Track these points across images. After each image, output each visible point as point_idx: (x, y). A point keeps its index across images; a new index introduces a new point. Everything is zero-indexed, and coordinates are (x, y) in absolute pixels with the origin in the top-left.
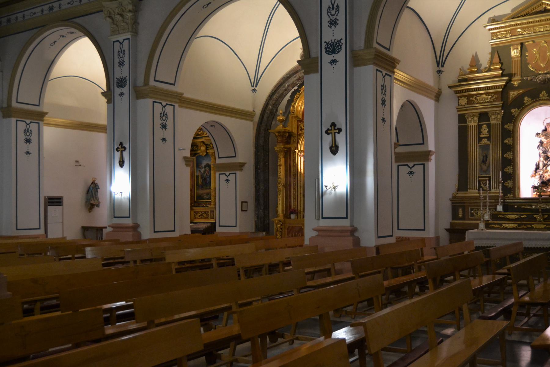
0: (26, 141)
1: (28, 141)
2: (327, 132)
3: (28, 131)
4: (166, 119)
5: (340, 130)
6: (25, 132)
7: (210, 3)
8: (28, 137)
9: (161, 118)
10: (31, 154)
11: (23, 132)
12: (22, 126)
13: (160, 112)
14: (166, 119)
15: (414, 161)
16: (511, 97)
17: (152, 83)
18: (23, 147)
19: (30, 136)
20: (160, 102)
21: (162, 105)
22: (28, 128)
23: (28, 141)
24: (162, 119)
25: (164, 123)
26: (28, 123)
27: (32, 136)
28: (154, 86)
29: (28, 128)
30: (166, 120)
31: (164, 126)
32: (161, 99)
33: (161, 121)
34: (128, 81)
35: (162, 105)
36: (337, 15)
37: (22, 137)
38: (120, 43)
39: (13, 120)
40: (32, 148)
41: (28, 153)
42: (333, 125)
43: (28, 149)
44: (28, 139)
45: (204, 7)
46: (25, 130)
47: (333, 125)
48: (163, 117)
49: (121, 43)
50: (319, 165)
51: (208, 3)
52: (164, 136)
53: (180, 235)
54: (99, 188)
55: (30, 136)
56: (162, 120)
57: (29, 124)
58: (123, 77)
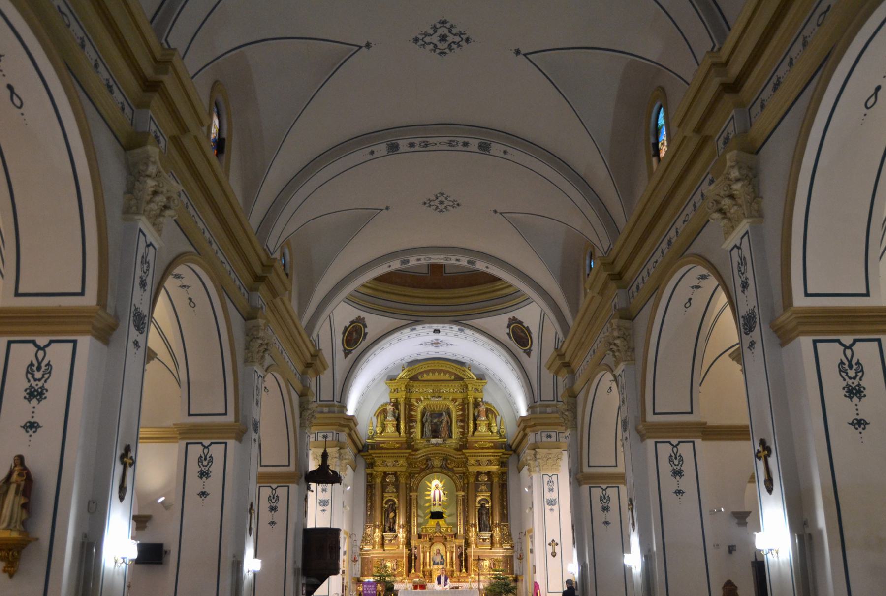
0: (675, 473)
1: (678, 473)
2: (550, 545)
4: (147, 272)
5: (557, 544)
7: (878, 88)
9: (844, 374)
11: (838, 369)
12: (665, 450)
14: (147, 272)
18: (669, 484)
21: (672, 445)
22: (675, 452)
23: (678, 473)
24: (847, 375)
25: (144, 278)
26: (848, 345)
30: (147, 274)
31: (854, 391)
32: (670, 437)
33: (845, 380)
34: (757, 317)
35: (672, 445)
37: (666, 468)
38: (36, 345)
39: (650, 443)
40: (687, 482)
42: (553, 541)
43: (33, 417)
45: (869, 105)
47: (553, 541)
48: (849, 371)
49: (739, 248)
51: (873, 91)
52: (678, 487)
54: (735, 550)
56: (846, 378)
57: (850, 347)
58: (750, 310)
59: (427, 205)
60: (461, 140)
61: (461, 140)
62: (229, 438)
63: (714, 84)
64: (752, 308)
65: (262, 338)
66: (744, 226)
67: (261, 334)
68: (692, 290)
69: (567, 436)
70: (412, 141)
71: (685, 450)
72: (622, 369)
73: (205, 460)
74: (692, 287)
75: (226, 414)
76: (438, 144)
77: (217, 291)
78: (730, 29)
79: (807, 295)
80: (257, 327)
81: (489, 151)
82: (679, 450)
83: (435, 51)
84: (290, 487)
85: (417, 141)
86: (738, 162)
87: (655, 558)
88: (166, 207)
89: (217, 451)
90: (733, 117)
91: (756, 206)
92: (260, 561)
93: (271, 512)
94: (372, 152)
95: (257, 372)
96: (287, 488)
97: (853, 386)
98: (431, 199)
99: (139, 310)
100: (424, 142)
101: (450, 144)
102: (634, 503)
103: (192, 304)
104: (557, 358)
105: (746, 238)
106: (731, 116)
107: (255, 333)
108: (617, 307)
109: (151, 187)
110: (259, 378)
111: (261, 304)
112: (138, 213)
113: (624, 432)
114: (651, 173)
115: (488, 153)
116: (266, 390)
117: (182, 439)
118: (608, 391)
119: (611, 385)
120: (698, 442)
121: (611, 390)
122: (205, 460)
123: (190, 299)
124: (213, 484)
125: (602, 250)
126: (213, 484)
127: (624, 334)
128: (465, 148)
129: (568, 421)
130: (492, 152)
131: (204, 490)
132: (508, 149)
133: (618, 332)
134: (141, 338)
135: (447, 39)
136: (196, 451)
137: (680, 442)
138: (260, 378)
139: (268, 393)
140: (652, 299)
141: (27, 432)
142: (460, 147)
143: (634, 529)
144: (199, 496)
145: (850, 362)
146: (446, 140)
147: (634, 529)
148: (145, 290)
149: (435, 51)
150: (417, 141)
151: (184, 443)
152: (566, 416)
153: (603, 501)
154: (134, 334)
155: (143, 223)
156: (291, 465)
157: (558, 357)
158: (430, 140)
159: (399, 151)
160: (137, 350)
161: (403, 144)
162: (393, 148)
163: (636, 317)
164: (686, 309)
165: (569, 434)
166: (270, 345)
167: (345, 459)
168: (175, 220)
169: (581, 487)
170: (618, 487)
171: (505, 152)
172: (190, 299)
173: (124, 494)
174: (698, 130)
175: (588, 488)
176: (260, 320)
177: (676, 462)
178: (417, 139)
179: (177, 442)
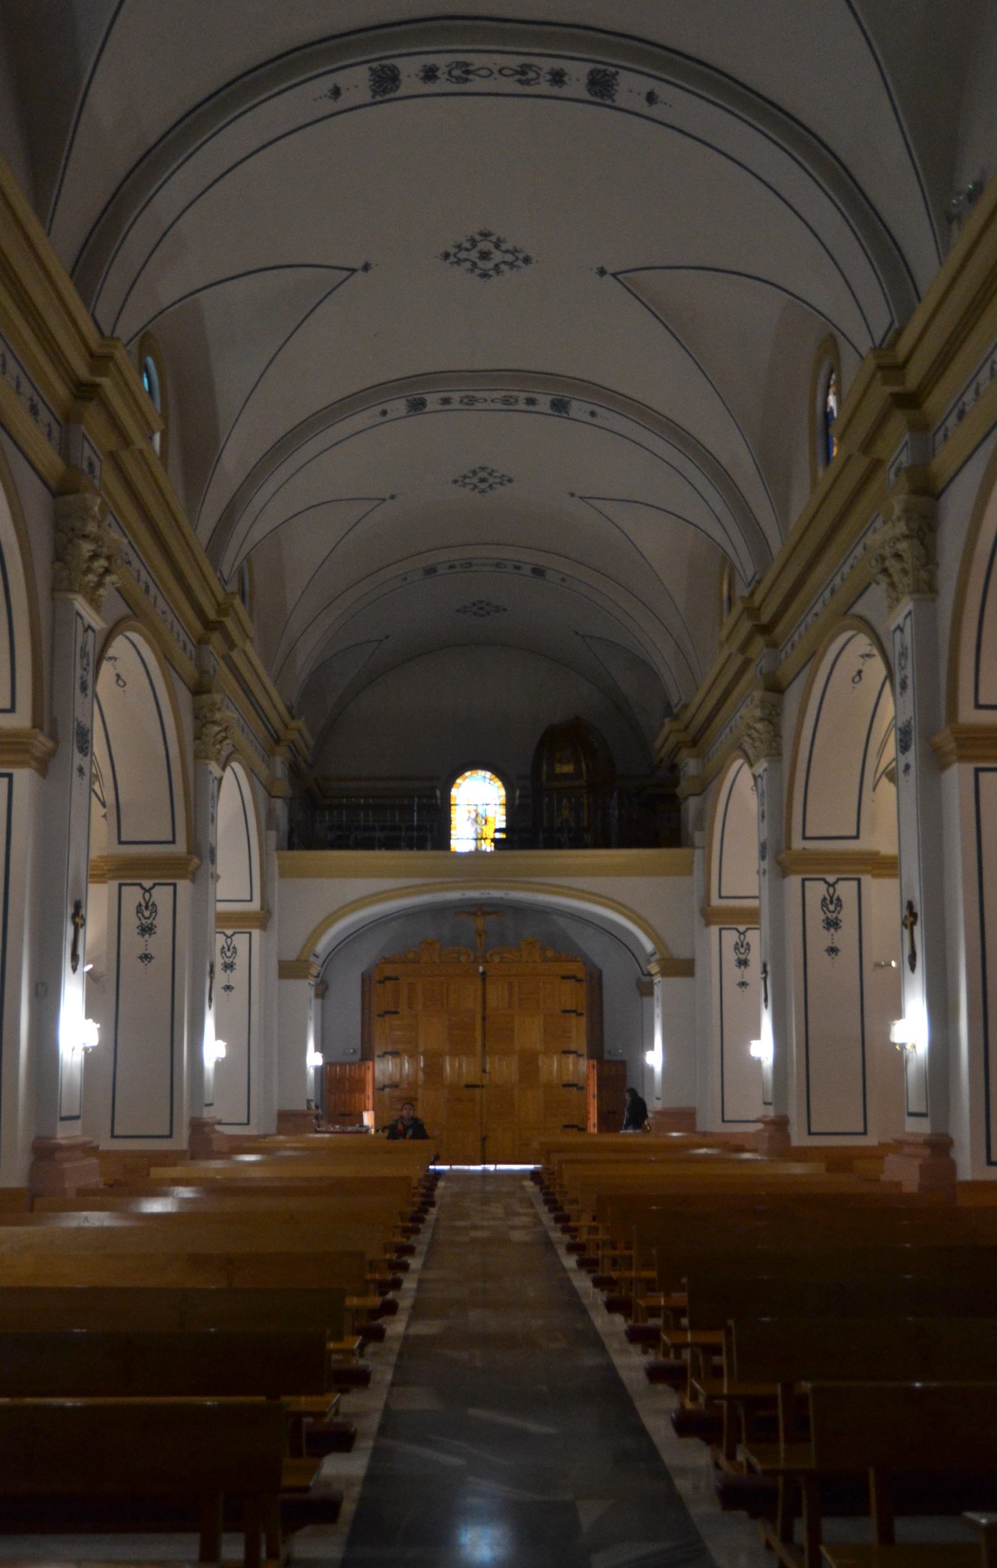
3: (742, 946)
6: (736, 947)
8: (147, 920)
10: (153, 961)
12: (730, 937)
13: (822, 897)
15: (234, 927)
16: (81, 543)
17: (798, 844)
18: (819, 938)
19: (152, 917)
20: (821, 876)
22: (147, 899)
27: (157, 918)
28: (804, 849)
29: (147, 899)
31: (832, 924)
36: (541, 69)
37: (730, 956)
39: (714, 929)
41: (743, 984)
43: (146, 950)
44: (146, 925)
46: (737, 944)
50: (21, 957)
53: (879, 1143)
55: (152, 917)
59: (521, 256)
60: (547, 65)
61: (547, 65)
62: (255, 927)
63: (882, 392)
64: (908, 718)
65: (96, 540)
66: (907, 604)
67: (91, 528)
68: (862, 660)
69: (760, 776)
70: (431, 60)
71: (846, 890)
72: (905, 612)
73: (147, 907)
74: (862, 656)
75: (173, 842)
76: (489, 400)
77: (249, 778)
78: (919, 299)
79: (978, 706)
80: (213, 707)
81: (611, 97)
82: (837, 890)
83: (499, 240)
84: (178, 887)
85: (442, 61)
86: (906, 510)
87: (797, 1047)
88: (107, 571)
89: (162, 896)
90: (906, 443)
91: (775, 745)
92: (225, 1044)
93: (143, 936)
94: (384, 413)
95: (81, 617)
96: (171, 888)
97: (832, 919)
98: (499, 486)
99: (373, 87)
100: (467, 397)
101: (506, 401)
102: (769, 968)
103: (121, 683)
104: (879, 375)
105: (909, 618)
106: (903, 443)
107: (208, 715)
108: (764, 672)
109: (89, 551)
110: (86, 631)
111: (89, 458)
112: (207, 758)
113: (903, 753)
114: (814, 482)
115: (565, 415)
116: (121, 683)
117: (114, 878)
118: (853, 681)
119: (863, 664)
120: (867, 880)
121: (861, 678)
122: (147, 907)
123: (118, 676)
124: (159, 943)
125: (745, 580)
126: (159, 943)
127: (770, 714)
128: (555, 91)
129: (762, 742)
130: (621, 99)
131: (228, 984)
132: (598, 410)
133: (907, 525)
134: (85, 763)
135: (437, 74)
136: (133, 896)
137: (838, 880)
138: (90, 632)
139: (125, 689)
140: (806, 671)
141: (143, 962)
142: (544, 87)
143: (766, 1007)
144: (140, 961)
145: (831, 898)
146: (514, 62)
147: (766, 1007)
148: (86, 695)
149: (499, 240)
150: (442, 61)
151: (115, 884)
152: (757, 731)
153: (828, 909)
154: (78, 759)
155: (80, 604)
156: (254, 900)
157: (879, 375)
158: (478, 395)
159: (399, 93)
160: (82, 779)
161: (432, 400)
162: (417, 405)
163: (952, 479)
164: (855, 685)
165: (765, 770)
166: (230, 729)
167: (214, 723)
168: (117, 589)
169: (786, 880)
170: (859, 880)
171: (593, 414)
172: (118, 676)
173: (77, 964)
174: (867, 445)
175: (800, 881)
176: (87, 495)
177: (832, 907)
178: (441, 56)
179: (105, 882)
